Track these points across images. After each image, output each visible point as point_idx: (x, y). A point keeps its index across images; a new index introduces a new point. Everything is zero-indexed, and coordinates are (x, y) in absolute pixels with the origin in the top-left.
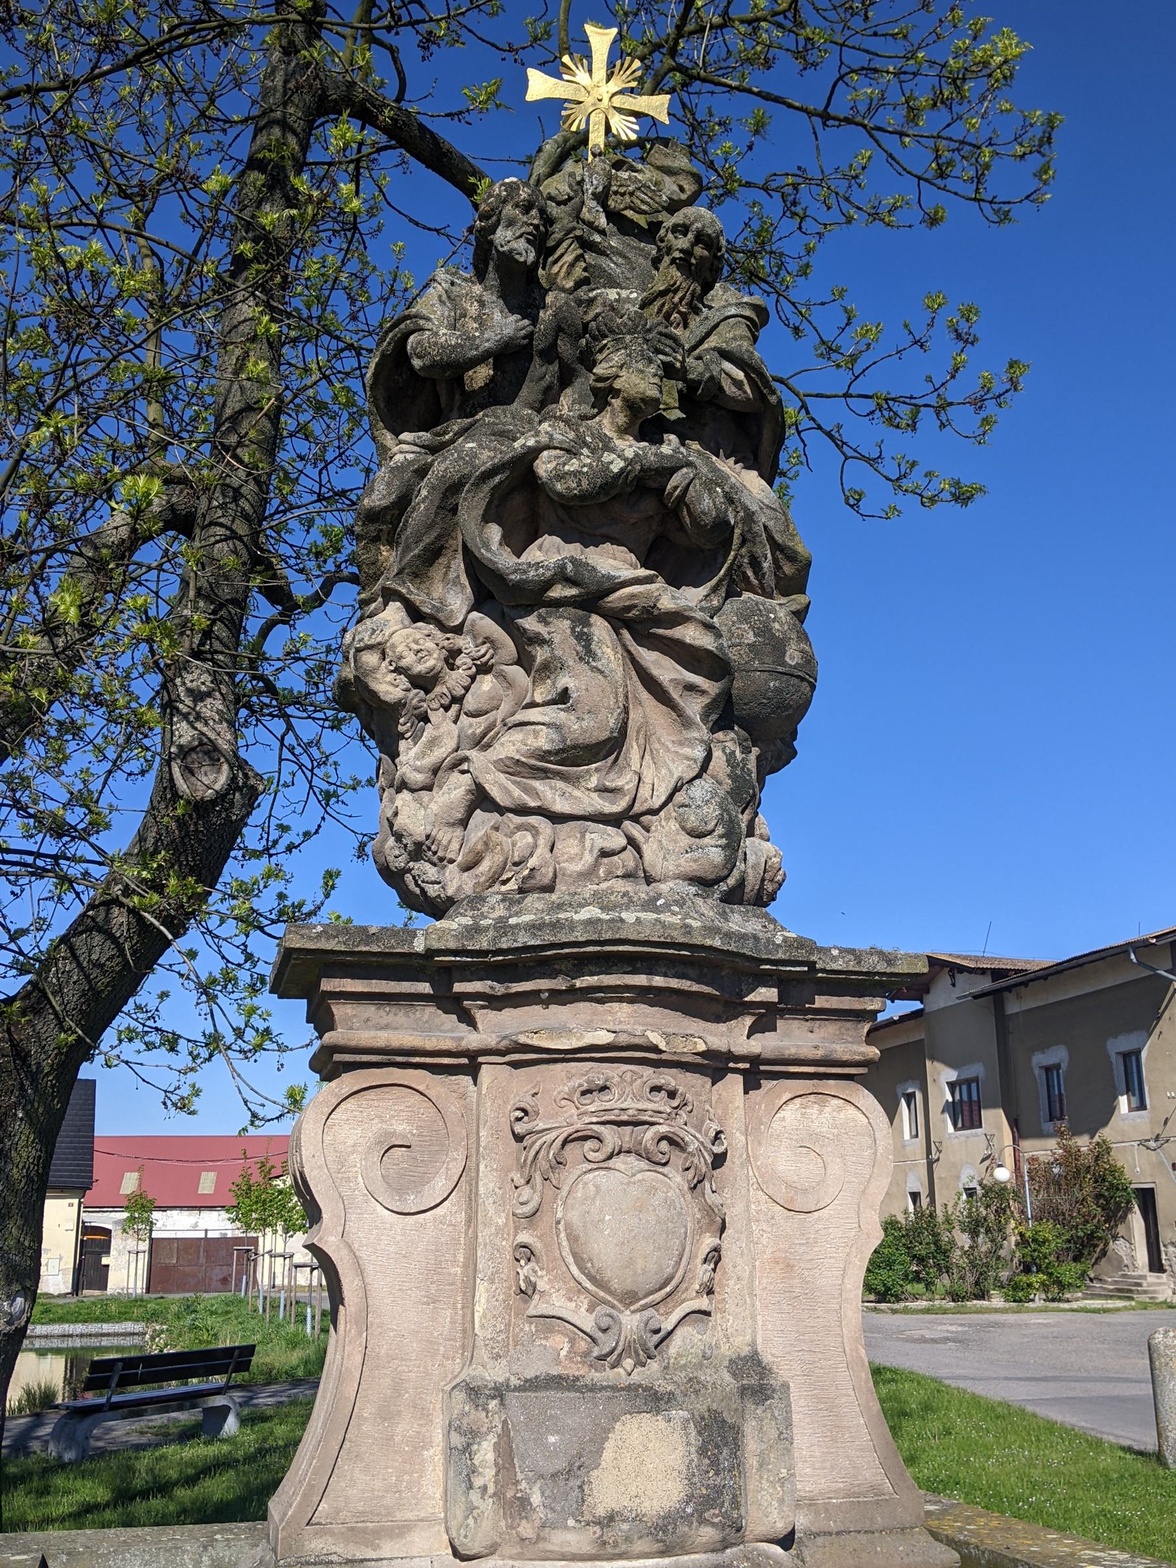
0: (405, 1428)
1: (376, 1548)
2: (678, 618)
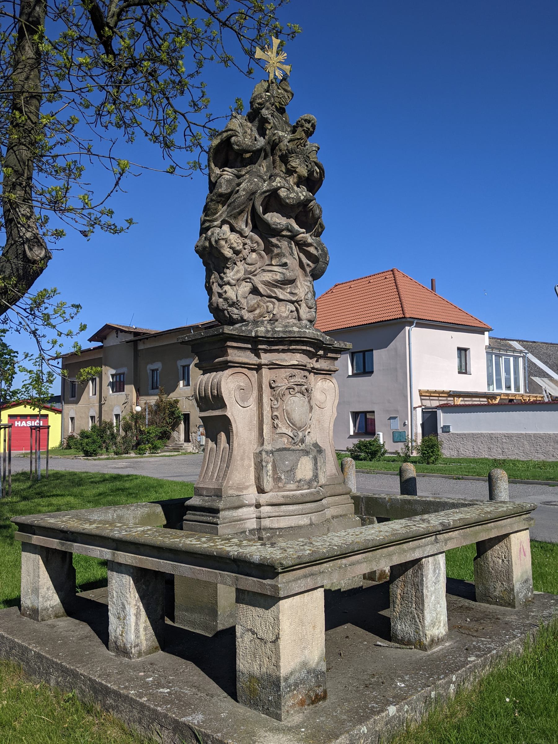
0: (246, 462)
1: (242, 492)
2: (310, 245)
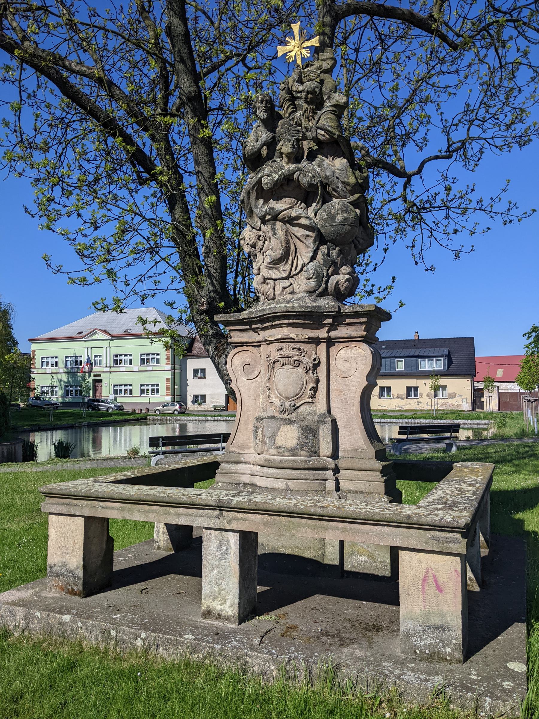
2: (298, 217)
